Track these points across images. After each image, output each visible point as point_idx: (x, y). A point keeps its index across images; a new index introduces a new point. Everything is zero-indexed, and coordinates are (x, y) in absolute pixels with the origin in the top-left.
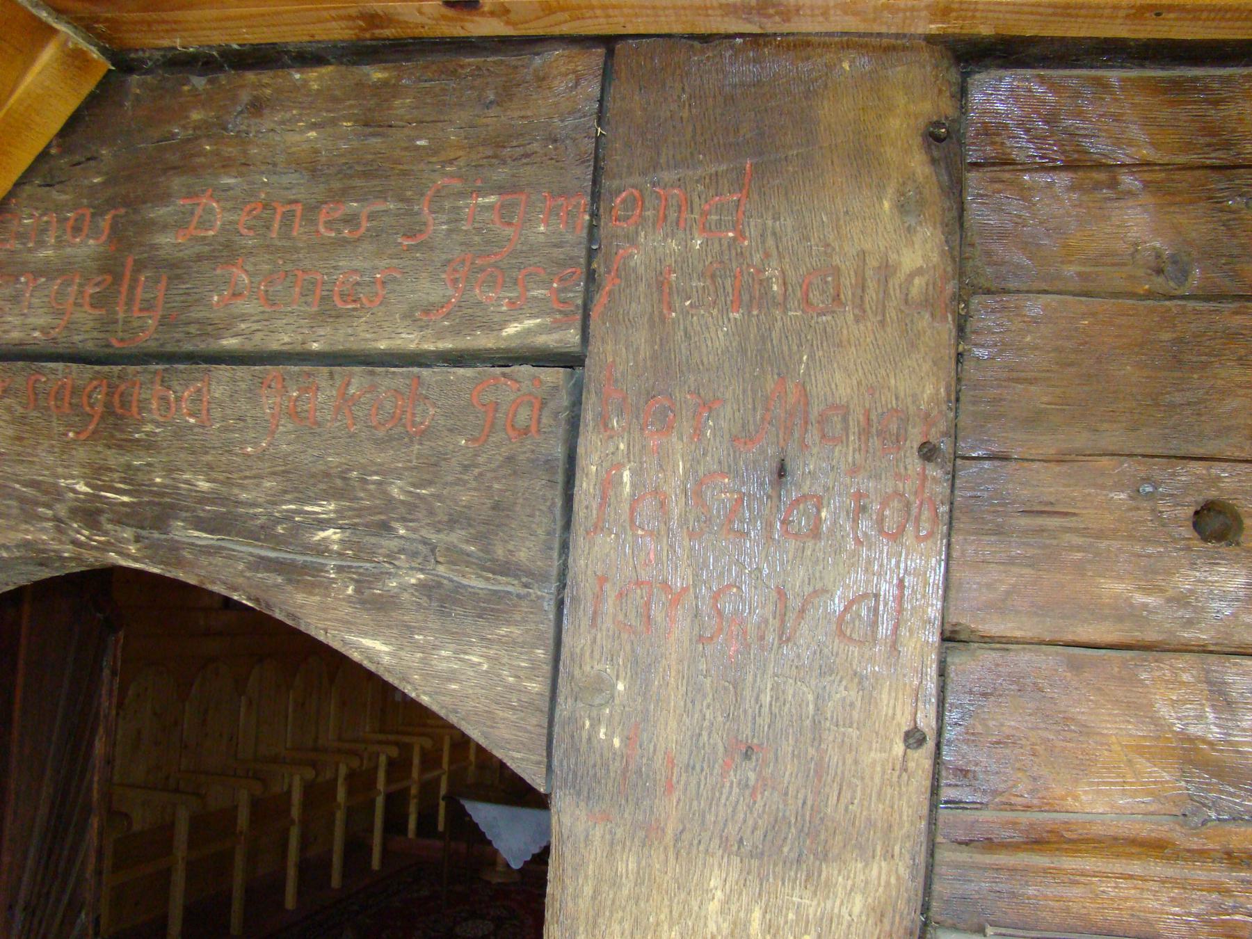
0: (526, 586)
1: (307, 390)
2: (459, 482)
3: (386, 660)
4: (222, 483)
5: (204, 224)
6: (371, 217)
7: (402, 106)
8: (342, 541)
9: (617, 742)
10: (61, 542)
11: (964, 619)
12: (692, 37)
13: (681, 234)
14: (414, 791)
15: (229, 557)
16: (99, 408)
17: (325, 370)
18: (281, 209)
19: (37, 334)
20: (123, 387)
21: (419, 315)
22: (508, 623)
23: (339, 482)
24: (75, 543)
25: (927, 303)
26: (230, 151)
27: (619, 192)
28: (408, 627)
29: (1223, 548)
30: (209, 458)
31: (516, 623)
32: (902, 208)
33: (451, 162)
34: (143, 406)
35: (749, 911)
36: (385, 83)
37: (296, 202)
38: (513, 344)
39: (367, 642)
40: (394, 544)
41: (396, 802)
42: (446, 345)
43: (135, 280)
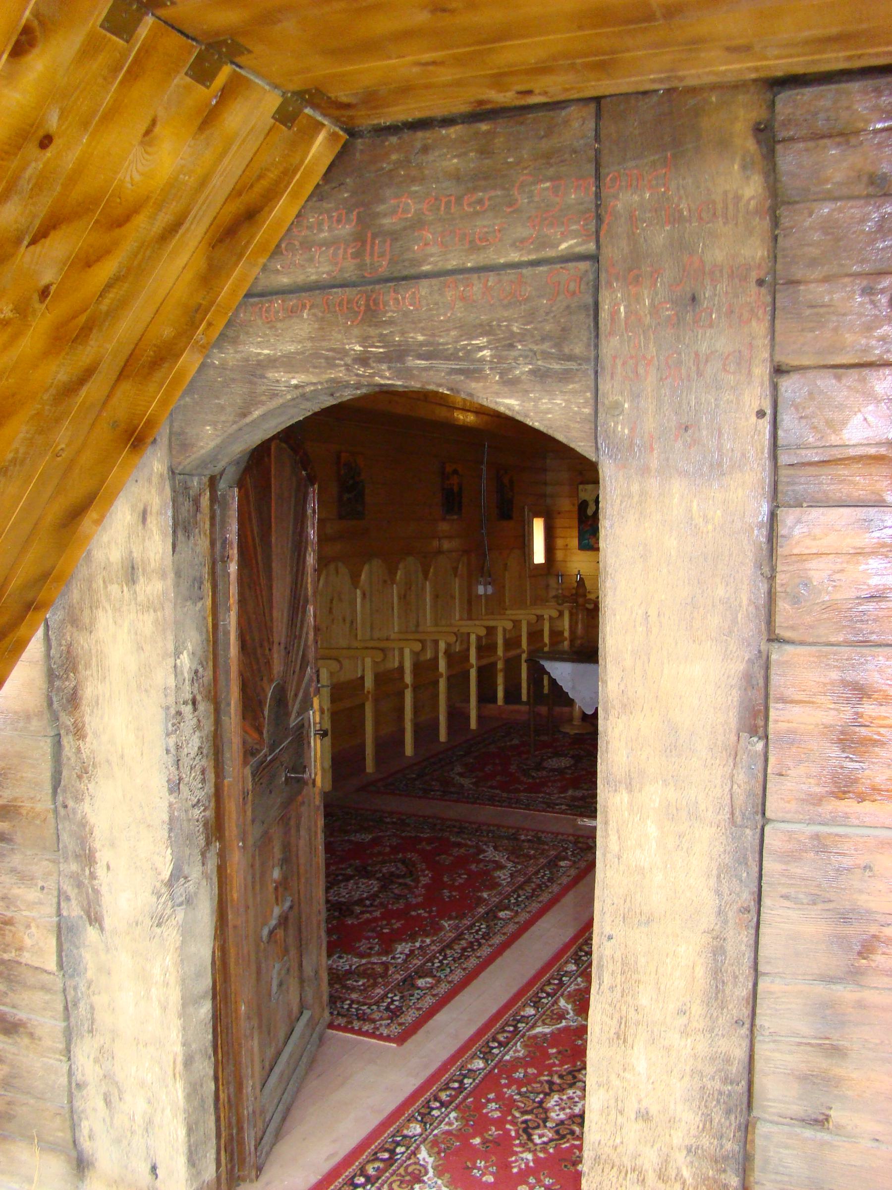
0: (580, 364)
1: (468, 286)
2: (545, 320)
3: (517, 408)
4: (430, 336)
5: (406, 211)
6: (490, 199)
7: (499, 141)
8: (491, 356)
9: (626, 431)
10: (350, 376)
11: (781, 358)
12: (638, 93)
13: (639, 193)
14: (500, 665)
15: (437, 371)
16: (362, 308)
17: (476, 276)
18: (444, 200)
19: (325, 276)
20: (374, 296)
21: (519, 244)
22: (573, 383)
23: (487, 328)
24: (357, 375)
25: (757, 212)
26: (414, 172)
27: (608, 174)
28: (527, 391)
30: (422, 325)
31: (576, 383)
32: (744, 167)
33: (526, 168)
34: (386, 304)
35: (691, 501)
36: (488, 132)
37: (451, 195)
38: (565, 253)
39: (507, 401)
40: (516, 353)
41: (486, 674)
42: (533, 257)
43: (373, 244)
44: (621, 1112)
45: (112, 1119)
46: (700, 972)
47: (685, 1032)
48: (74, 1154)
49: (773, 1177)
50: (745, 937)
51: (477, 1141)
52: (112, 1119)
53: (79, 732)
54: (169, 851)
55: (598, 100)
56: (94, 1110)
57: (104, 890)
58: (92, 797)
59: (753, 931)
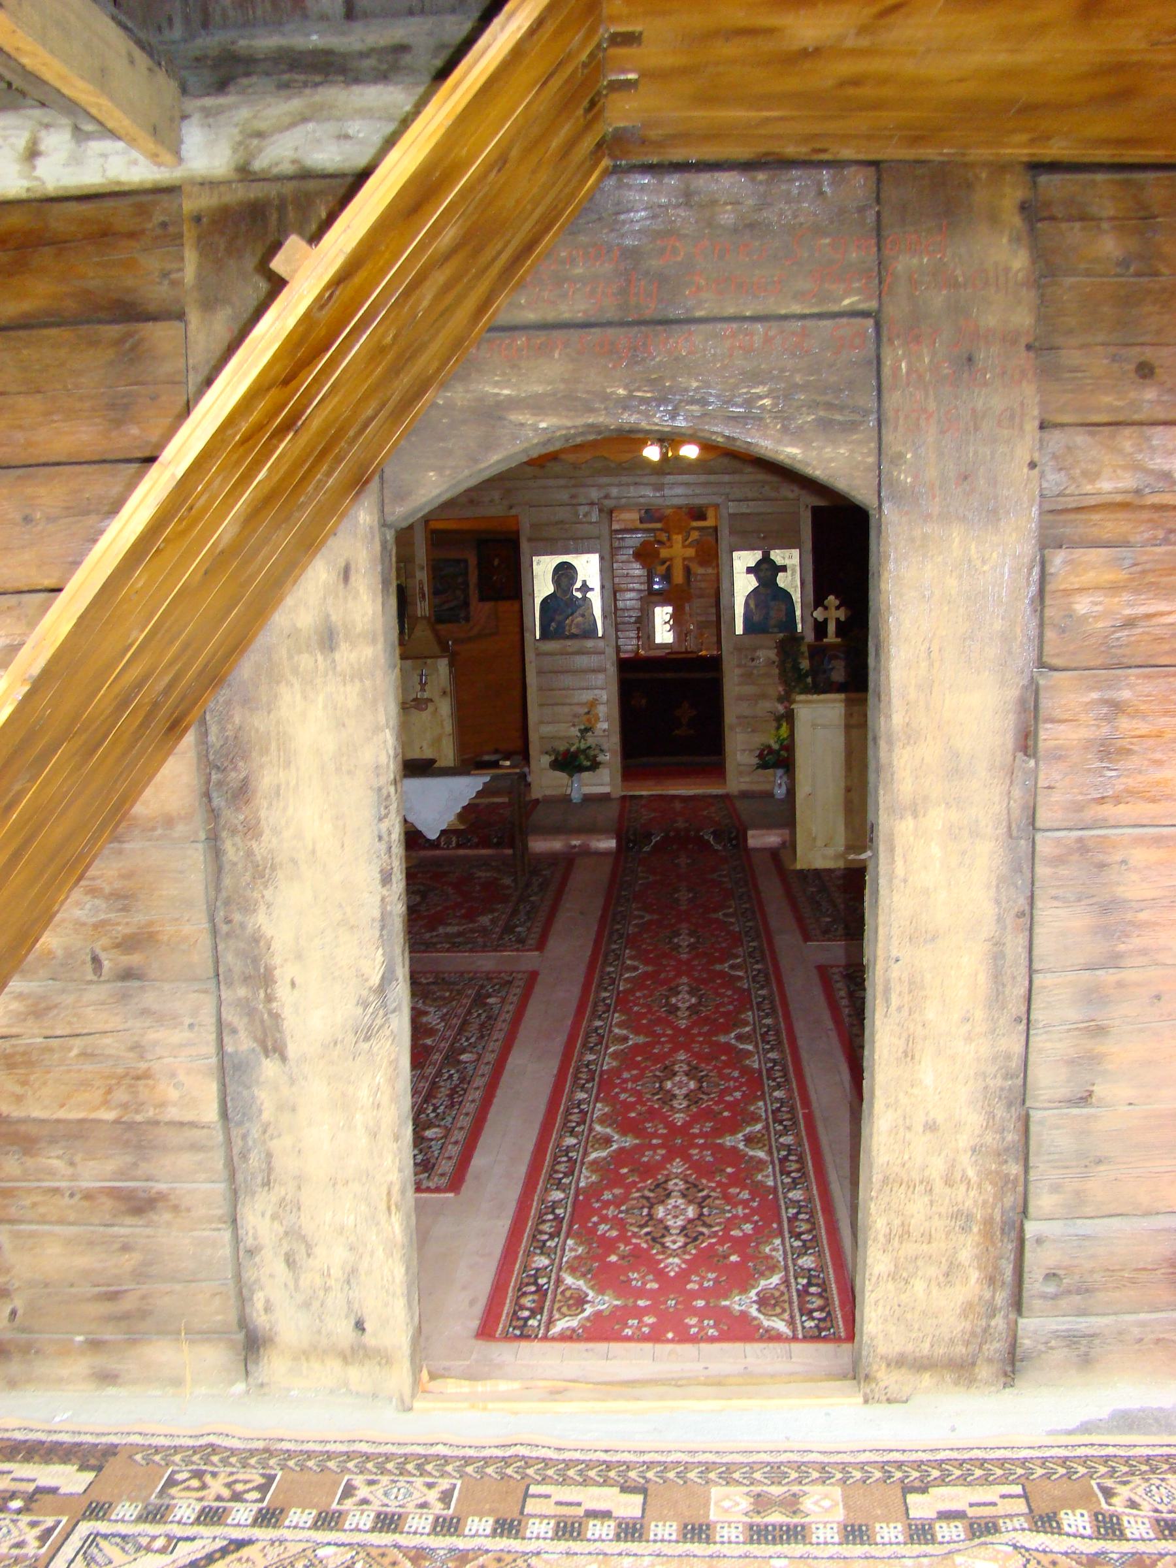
11: (1047, 417)
21: (799, 296)
29: (1147, 381)
42: (815, 310)
44: (909, 1128)
45: (296, 1281)
46: (982, 978)
47: (969, 1038)
48: (240, 1337)
49: (1046, 1158)
50: (1022, 940)
51: (613, 1258)
52: (296, 1281)
53: (252, 830)
54: (380, 951)
55: (875, 164)
56: (271, 1276)
57: (287, 1013)
58: (269, 905)
59: (1027, 933)
